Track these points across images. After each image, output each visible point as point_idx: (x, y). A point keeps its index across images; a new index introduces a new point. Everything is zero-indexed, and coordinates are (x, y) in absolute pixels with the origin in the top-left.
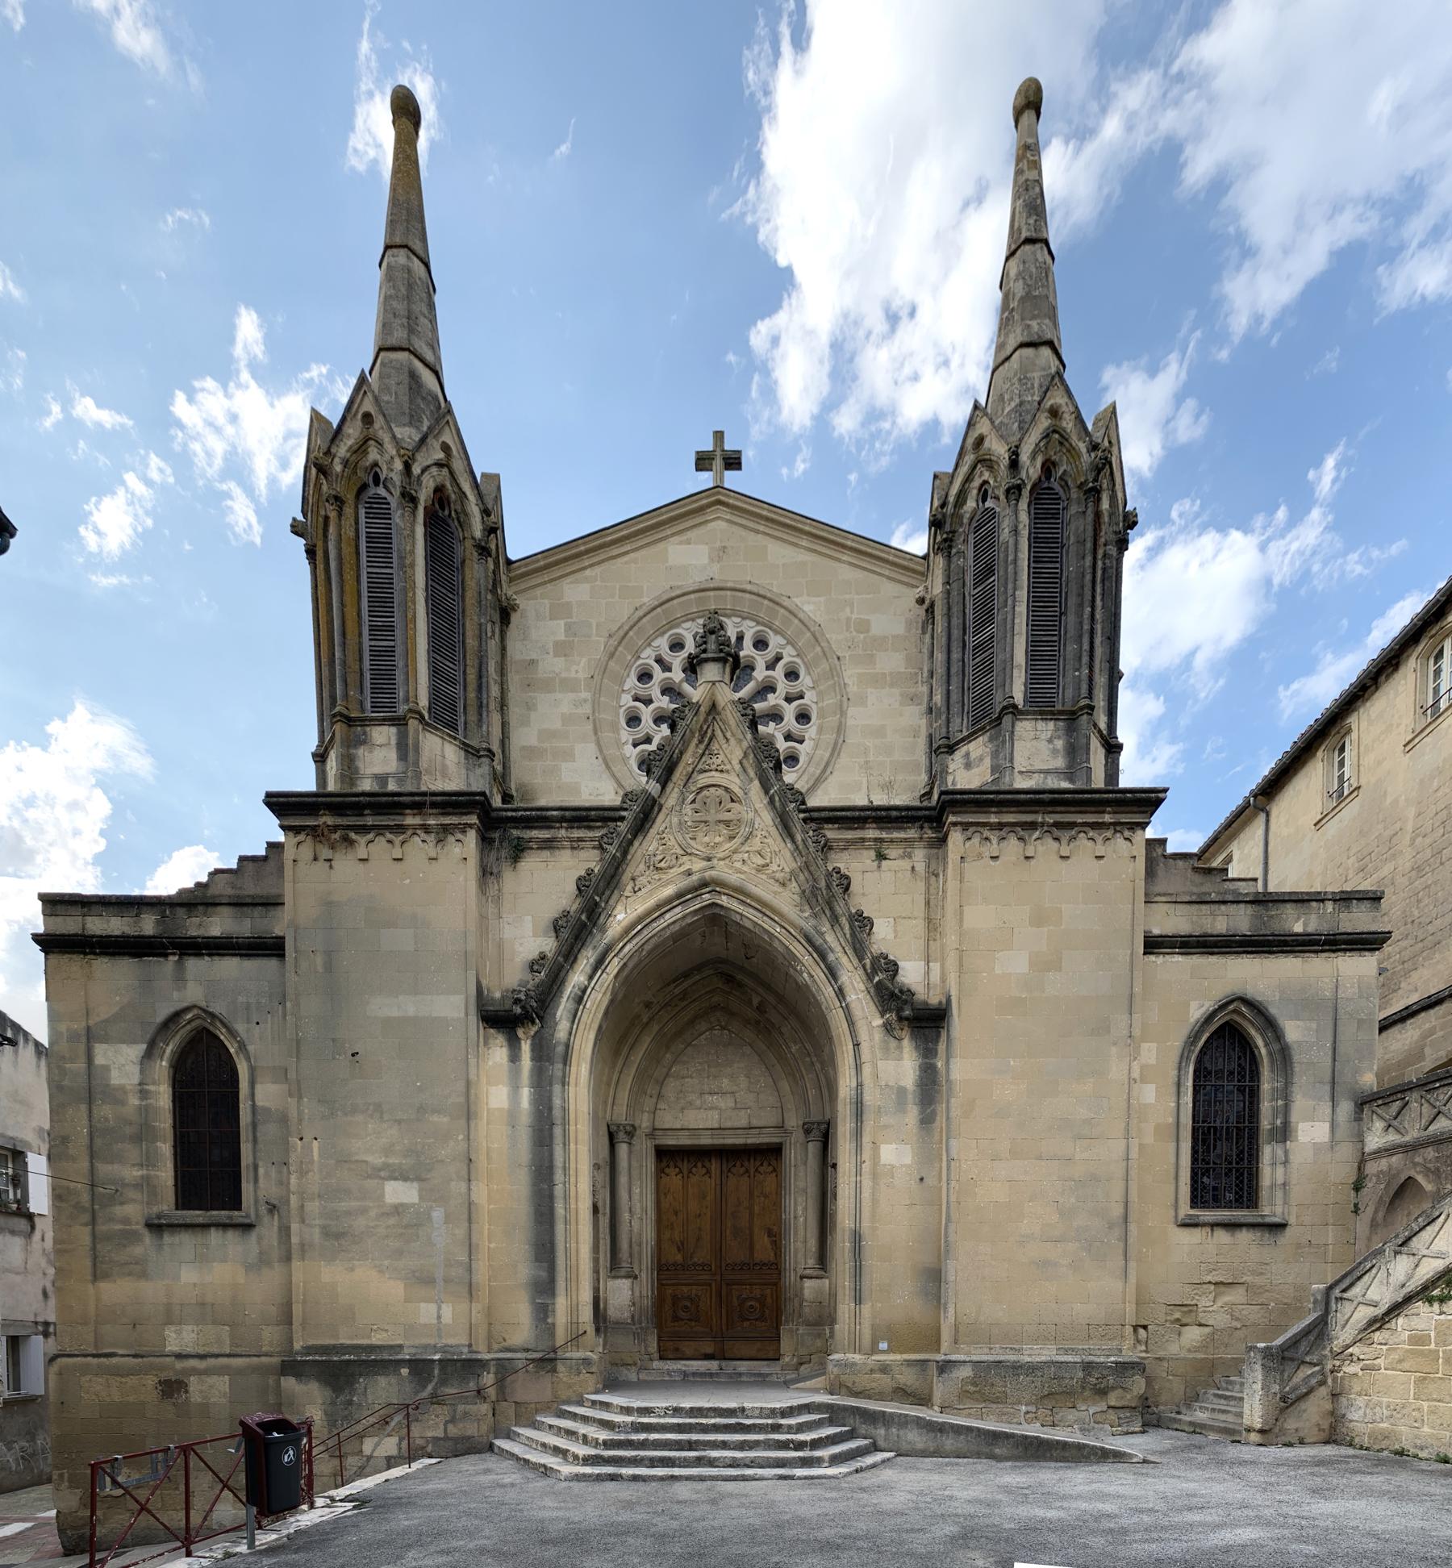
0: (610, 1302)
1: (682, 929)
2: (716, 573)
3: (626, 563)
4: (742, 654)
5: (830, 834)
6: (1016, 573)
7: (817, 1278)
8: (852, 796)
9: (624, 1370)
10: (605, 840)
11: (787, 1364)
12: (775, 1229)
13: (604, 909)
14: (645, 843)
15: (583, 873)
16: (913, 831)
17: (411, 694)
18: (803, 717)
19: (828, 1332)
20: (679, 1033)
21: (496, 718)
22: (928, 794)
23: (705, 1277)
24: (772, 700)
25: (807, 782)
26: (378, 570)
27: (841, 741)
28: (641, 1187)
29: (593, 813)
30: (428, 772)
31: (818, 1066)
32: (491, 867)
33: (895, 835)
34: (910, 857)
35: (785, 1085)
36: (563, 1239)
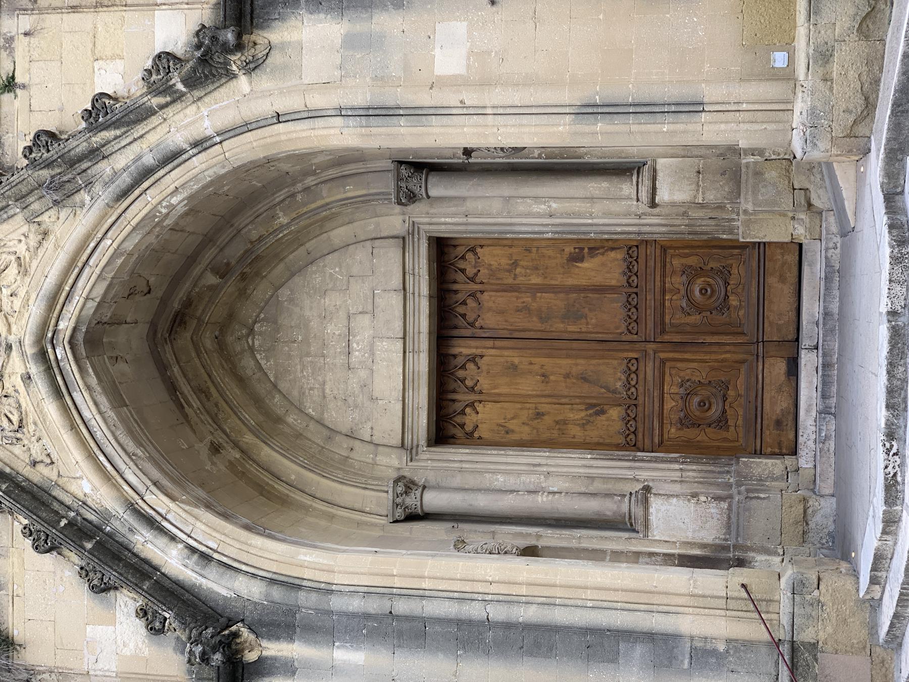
0: (689, 536)
1: (105, 391)
7: (654, 179)
9: (816, 520)
11: (809, 230)
12: (569, 249)
13: (78, 514)
15: (28, 542)
19: (751, 159)
20: (258, 402)
23: (650, 369)
28: (494, 472)
31: (310, 181)
35: (339, 234)
36: (579, 612)
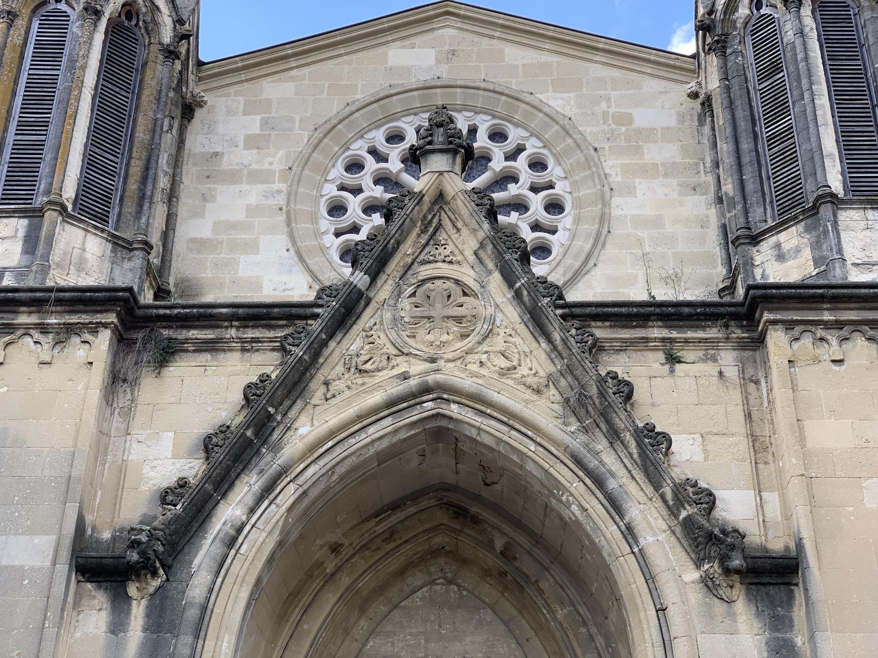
1: (392, 446)
2: (444, 72)
3: (339, 64)
4: (475, 145)
5: (599, 333)
6: (809, 70)
8: (626, 291)
10: (290, 340)
13: (279, 423)
14: (345, 342)
15: (254, 379)
16: (715, 330)
17: (55, 185)
18: (554, 207)
20: (381, 589)
21: (160, 212)
22: (731, 288)
24: (513, 189)
25: (564, 275)
26: (42, 72)
27: (605, 231)
29: (276, 310)
30: (58, 265)
31: (600, 641)
32: (126, 373)
33: (690, 334)
34: (714, 359)
